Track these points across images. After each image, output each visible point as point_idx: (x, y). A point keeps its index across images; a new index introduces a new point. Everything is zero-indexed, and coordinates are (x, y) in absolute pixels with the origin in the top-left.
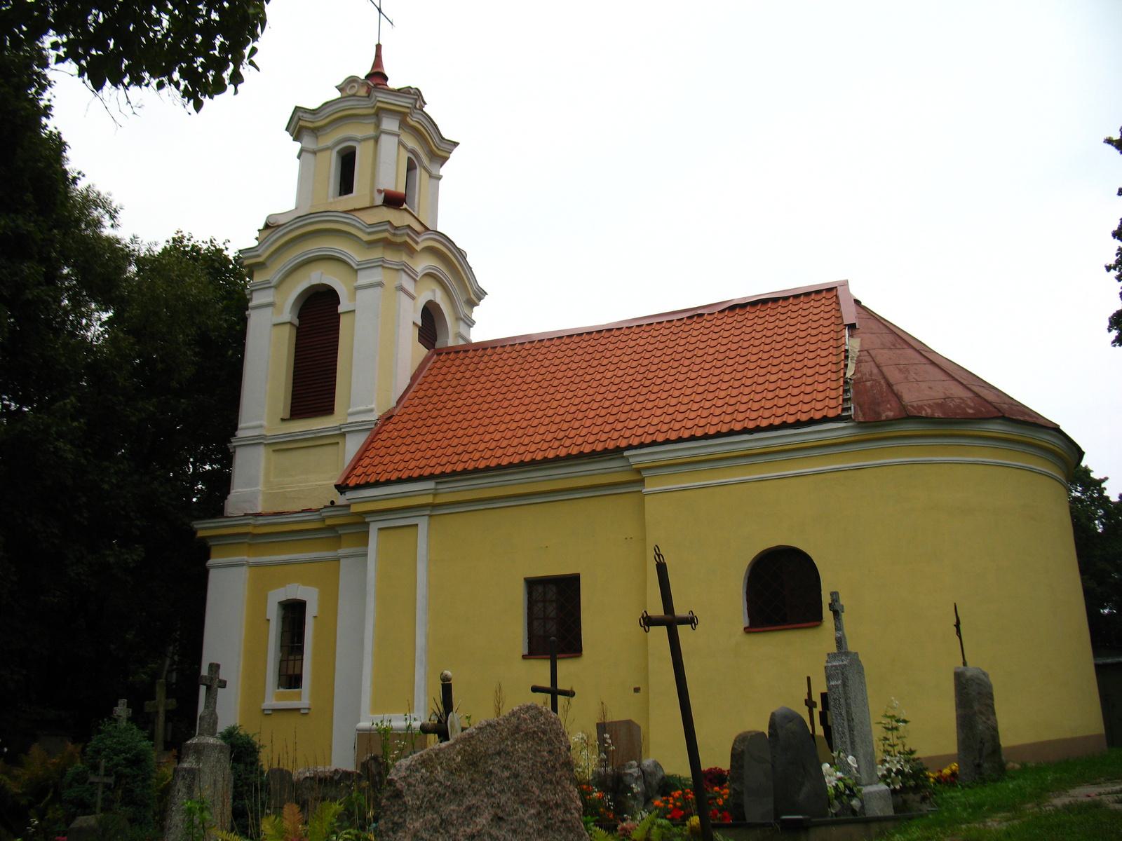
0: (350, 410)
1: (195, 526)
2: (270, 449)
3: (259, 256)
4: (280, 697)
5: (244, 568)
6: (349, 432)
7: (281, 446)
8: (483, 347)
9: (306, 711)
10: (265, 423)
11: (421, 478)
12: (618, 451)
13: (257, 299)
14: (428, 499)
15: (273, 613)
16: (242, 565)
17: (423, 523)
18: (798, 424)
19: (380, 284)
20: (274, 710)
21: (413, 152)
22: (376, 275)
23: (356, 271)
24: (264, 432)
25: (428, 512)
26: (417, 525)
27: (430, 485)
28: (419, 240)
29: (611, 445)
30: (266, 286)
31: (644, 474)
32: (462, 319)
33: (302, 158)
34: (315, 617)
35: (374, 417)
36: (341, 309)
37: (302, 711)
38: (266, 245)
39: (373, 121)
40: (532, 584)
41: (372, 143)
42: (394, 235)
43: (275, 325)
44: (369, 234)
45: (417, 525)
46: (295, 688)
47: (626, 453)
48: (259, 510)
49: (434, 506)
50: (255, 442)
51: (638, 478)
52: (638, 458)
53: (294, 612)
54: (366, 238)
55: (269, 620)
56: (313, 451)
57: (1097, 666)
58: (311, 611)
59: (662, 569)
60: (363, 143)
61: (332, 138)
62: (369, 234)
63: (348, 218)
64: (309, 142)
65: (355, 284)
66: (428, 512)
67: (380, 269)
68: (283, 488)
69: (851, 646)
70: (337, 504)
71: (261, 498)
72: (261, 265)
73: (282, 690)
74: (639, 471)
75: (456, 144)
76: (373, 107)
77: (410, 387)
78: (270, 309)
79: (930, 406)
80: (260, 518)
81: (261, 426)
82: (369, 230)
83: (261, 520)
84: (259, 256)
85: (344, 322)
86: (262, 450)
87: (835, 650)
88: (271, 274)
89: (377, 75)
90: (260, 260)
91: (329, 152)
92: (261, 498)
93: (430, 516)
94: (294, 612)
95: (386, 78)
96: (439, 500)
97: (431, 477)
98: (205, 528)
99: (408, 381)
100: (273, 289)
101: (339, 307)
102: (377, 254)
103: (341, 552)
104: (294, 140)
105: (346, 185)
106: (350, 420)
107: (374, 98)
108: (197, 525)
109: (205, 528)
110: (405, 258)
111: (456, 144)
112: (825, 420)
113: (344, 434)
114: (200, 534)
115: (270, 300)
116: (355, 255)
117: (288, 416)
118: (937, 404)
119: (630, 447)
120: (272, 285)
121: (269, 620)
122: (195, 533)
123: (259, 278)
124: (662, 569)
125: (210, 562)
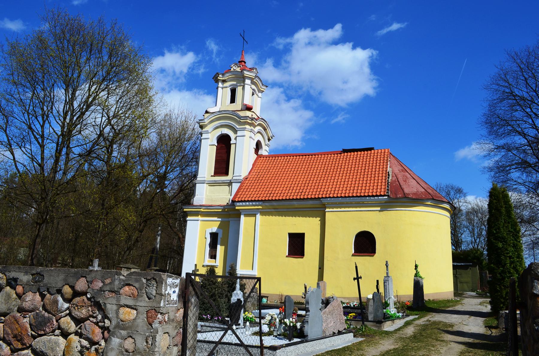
7: (212, 184)
21: (253, 90)
24: (205, 179)
28: (257, 122)
32: (267, 145)
35: (242, 178)
36: (231, 142)
47: (321, 199)
50: (203, 182)
57: (453, 265)
59: (356, 267)
69: (390, 275)
71: (204, 199)
77: (252, 168)
79: (412, 194)
84: (205, 122)
87: (386, 276)
92: (204, 199)
99: (251, 167)
101: (231, 142)
104: (215, 82)
105: (233, 100)
110: (252, 128)
117: (213, 174)
118: (414, 193)
124: (356, 267)
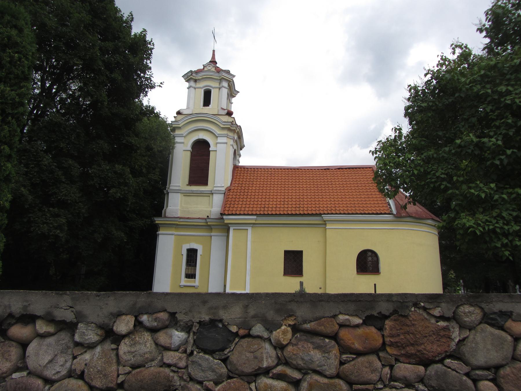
0: (215, 185)
1: (155, 219)
2: (183, 195)
3: (179, 124)
4: (186, 281)
5: (174, 236)
6: (214, 193)
8: (244, 168)
9: (197, 287)
10: (180, 185)
11: (252, 215)
12: (320, 214)
13: (177, 140)
14: (254, 222)
15: (185, 253)
16: (173, 235)
17: (250, 229)
18: (377, 214)
19: (226, 143)
20: (184, 286)
22: (224, 140)
23: (217, 137)
24: (180, 188)
25: (252, 226)
26: (248, 229)
27: (255, 217)
29: (318, 212)
30: (181, 136)
31: (327, 222)
33: (189, 89)
34: (201, 255)
36: (210, 149)
37: (196, 287)
38: (183, 121)
39: (219, 81)
40: (287, 253)
41: (218, 89)
42: (231, 126)
43: (184, 150)
44: (224, 125)
45: (248, 229)
46: (191, 278)
48: (179, 216)
49: (254, 224)
51: (325, 223)
52: (326, 217)
53: (192, 254)
54: (222, 126)
55: (183, 255)
56: (199, 198)
58: (199, 253)
60: (214, 89)
61: (203, 84)
62: (224, 125)
63: (213, 117)
64: (192, 84)
65: (217, 142)
66: (252, 226)
67: (226, 137)
68: (188, 209)
70: (209, 217)
72: (179, 128)
73: (186, 279)
74: (325, 221)
75: (238, 92)
76: (220, 77)
78: (182, 144)
80: (181, 219)
81: (179, 186)
82: (223, 124)
83: (182, 220)
84: (179, 124)
85: (212, 154)
86: (179, 195)
88: (184, 131)
89: (213, 62)
90: (180, 126)
91: (201, 89)
92: (179, 211)
93: (252, 227)
94: (192, 254)
95: (216, 63)
96: (256, 222)
97: (256, 215)
98: (158, 221)
100: (183, 137)
102: (225, 132)
103: (212, 234)
106: (215, 189)
107: (221, 74)
108: (156, 219)
109: (158, 221)
111: (238, 92)
112: (385, 214)
113: (213, 194)
114: (157, 222)
115: (182, 141)
116: (218, 131)
117: (188, 184)
119: (324, 214)
120: (183, 136)
121: (183, 255)
122: (155, 221)
123: (177, 132)
125: (159, 232)
